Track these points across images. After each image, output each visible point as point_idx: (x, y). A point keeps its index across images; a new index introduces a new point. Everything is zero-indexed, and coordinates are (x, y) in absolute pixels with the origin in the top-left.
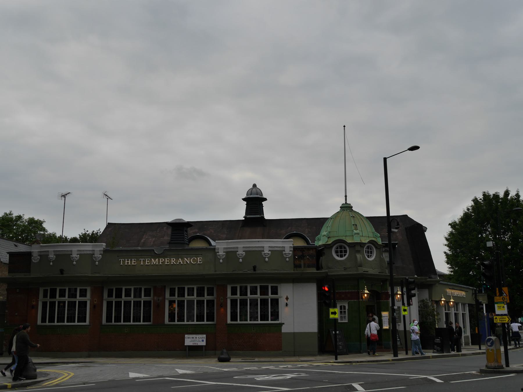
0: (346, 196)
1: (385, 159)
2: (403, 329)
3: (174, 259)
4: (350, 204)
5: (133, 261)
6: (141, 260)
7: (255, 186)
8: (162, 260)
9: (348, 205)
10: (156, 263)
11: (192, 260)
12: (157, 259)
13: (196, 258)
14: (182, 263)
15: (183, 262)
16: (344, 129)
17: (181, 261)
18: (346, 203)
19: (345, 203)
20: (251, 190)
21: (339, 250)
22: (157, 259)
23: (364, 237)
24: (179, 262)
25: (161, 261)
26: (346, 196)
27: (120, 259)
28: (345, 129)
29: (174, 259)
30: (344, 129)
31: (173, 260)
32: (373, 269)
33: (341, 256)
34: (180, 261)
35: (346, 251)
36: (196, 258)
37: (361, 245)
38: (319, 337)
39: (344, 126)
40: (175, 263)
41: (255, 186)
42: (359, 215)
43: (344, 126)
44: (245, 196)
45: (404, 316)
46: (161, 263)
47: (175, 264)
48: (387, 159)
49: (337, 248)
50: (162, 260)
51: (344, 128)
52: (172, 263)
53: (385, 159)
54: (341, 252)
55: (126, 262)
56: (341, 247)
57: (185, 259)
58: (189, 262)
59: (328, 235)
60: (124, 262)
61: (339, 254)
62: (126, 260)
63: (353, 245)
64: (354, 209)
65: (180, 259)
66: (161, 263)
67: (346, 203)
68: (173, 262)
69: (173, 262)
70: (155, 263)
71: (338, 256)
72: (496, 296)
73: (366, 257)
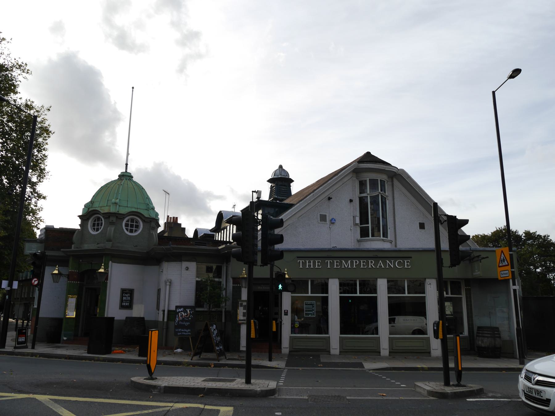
0: (127, 165)
1: (494, 93)
2: (161, 320)
3: (373, 261)
4: (130, 173)
5: (317, 264)
6: (300, 262)
7: (281, 167)
8: (356, 262)
9: (128, 174)
10: (348, 266)
11: (398, 262)
12: (349, 261)
13: (402, 261)
14: (383, 267)
15: (385, 265)
16: (133, 90)
17: (382, 265)
18: (126, 171)
19: (125, 171)
20: (274, 173)
21: (130, 223)
22: (349, 261)
23: (108, 206)
24: (379, 265)
25: (354, 264)
26: (127, 165)
27: (326, 261)
28: (134, 91)
29: (372, 262)
30: (133, 90)
31: (372, 262)
32: (134, 246)
33: (131, 231)
34: (380, 264)
35: (137, 227)
36: (402, 261)
37: (117, 217)
38: (439, 312)
39: (133, 88)
40: (374, 267)
41: (281, 167)
42: (140, 189)
43: (133, 88)
44: (270, 177)
45: (515, 291)
46: (378, 266)
47: (374, 268)
48: (495, 92)
49: (128, 221)
50: (356, 262)
51: (132, 89)
52: (370, 267)
53: (494, 93)
54: (132, 226)
55: (307, 264)
56: (132, 220)
57: (388, 261)
58: (392, 266)
59: (90, 205)
60: (304, 264)
61: (96, 227)
62: (307, 261)
63: (108, 215)
64: (134, 179)
65: (380, 261)
66: (378, 266)
67: (126, 171)
68: (371, 265)
69: (371, 265)
70: (346, 266)
71: (136, 231)
72: (256, 265)
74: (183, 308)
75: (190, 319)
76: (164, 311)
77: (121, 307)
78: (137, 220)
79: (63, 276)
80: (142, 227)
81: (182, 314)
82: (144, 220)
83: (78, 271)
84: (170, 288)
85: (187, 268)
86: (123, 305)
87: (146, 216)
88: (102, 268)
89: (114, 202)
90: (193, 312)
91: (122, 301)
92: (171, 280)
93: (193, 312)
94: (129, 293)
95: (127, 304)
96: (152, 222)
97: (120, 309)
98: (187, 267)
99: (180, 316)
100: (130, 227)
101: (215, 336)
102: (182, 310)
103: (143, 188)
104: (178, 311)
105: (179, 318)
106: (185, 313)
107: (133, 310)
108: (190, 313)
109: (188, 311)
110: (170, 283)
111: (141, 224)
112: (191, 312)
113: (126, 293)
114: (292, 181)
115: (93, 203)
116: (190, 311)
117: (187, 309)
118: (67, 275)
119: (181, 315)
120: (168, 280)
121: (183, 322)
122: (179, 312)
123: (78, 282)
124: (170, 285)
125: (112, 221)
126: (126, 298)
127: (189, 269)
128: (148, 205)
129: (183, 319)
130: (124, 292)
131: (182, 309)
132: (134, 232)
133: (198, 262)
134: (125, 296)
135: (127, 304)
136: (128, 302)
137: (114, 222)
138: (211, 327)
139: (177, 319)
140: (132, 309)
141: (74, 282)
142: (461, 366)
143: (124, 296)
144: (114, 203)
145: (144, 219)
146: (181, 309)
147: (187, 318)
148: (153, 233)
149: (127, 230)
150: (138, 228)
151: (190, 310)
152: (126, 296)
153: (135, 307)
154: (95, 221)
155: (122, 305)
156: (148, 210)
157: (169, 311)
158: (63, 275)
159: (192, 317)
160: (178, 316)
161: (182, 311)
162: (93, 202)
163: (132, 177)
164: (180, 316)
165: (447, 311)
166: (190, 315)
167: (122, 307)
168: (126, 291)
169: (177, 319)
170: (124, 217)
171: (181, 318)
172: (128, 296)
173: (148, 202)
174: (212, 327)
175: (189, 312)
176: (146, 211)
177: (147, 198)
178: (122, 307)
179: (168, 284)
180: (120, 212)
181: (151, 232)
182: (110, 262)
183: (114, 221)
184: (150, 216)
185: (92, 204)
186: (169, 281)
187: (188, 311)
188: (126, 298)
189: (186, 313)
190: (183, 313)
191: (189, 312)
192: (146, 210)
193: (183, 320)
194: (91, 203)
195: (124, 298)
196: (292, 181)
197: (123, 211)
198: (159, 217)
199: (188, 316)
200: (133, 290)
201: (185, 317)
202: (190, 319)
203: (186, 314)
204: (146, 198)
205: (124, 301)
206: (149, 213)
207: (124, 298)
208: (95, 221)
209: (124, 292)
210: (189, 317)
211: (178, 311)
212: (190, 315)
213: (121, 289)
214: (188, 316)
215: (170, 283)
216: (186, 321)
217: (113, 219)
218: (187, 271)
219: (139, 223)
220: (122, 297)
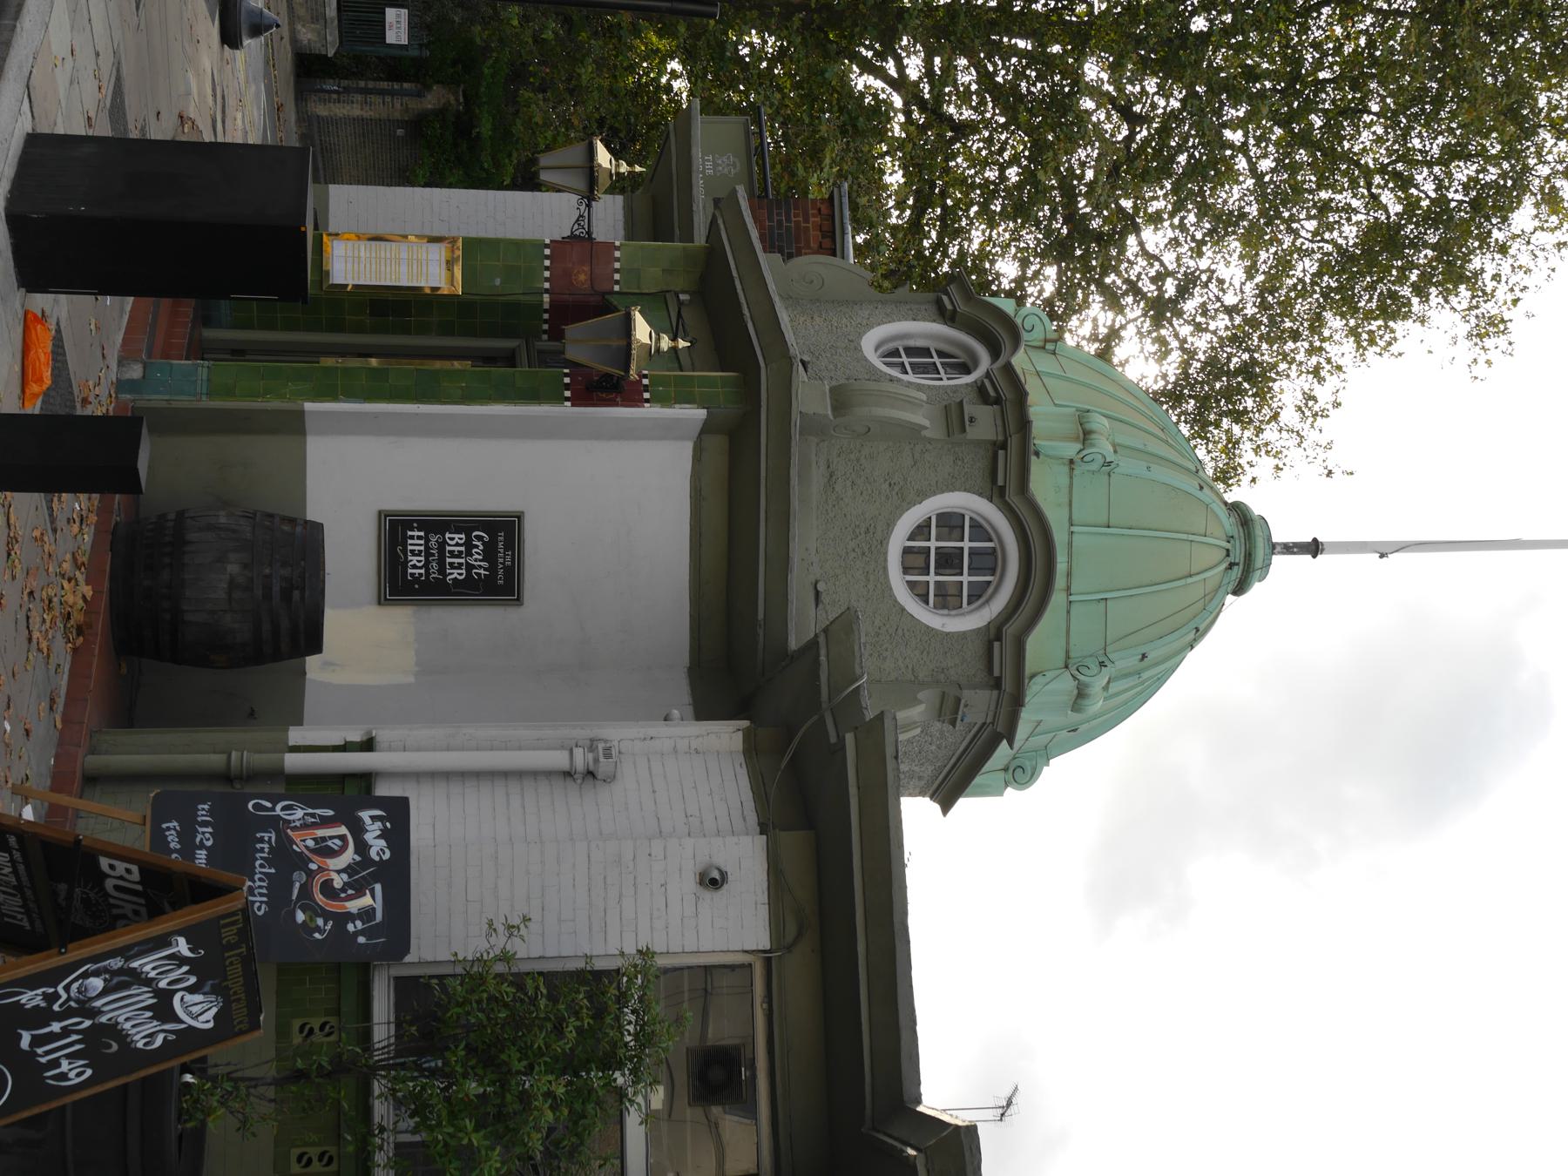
4: (1267, 566)
18: (1273, 548)
21: (966, 545)
33: (914, 560)
35: (946, 600)
49: (980, 530)
56: (988, 561)
67: (1273, 548)
73: (898, 539)
74: (387, 856)
75: (300, 917)
76: (368, 745)
77: (395, 590)
78: (990, 590)
79: (583, 208)
80: (948, 629)
81: (333, 853)
82: (999, 638)
83: (617, 288)
84: (549, 774)
85: (716, 875)
86: (405, 538)
87: (1032, 643)
88: (658, 339)
89: (1093, 426)
90: (361, 940)
91: (436, 524)
92: (610, 779)
93: (361, 940)
94: (492, 568)
95: (414, 560)
96: (995, 692)
97: (383, 515)
98: (724, 875)
99: (321, 833)
100: (937, 548)
101: (84, 1008)
102: (373, 854)
103: (1199, 634)
104: (365, 815)
105: (305, 826)
106: (345, 877)
107: (375, 610)
108: (350, 917)
109: (366, 901)
110: (590, 774)
111: (968, 618)
112: (359, 924)
113: (490, 554)
114: (1314, 557)
115: (1048, 352)
116: (367, 914)
117: (378, 887)
118: (589, 233)
119: (335, 844)
120: (608, 755)
121: (268, 862)
122: (358, 829)
123: (546, 298)
124: (568, 774)
125: (972, 420)
126: (459, 555)
127: (708, 895)
128: (1102, 664)
129: (301, 862)
130: (501, 537)
131: (378, 847)
132: (908, 582)
133: (768, 961)
134: (469, 546)
135: (414, 560)
136: (426, 566)
137: (964, 430)
138: (182, 946)
139: (299, 813)
140: (382, 601)
141: (546, 316)
142: (1001, 645)
143: (469, 539)
144: (1088, 426)
145: (1010, 630)
146: (382, 843)
147: (306, 890)
148: (915, 702)
149: (921, 531)
150: (935, 607)
151: (379, 916)
152: (469, 554)
153: (401, 620)
154: (941, 354)
155: (408, 525)
156: (1066, 667)
157: (366, 779)
158: (589, 206)
159: (318, 929)
160: (325, 822)
161: (362, 847)
162: (1054, 353)
163: (1240, 589)
164: (321, 833)
165: (580, 11)
166: (327, 916)
167: (395, 528)
168: (509, 545)
169: (299, 813)
170: (1002, 490)
171: (303, 842)
172: (470, 567)
173: (1120, 664)
174: (195, 966)
175: (354, 906)
176: (1062, 655)
177: (1144, 656)
178: (395, 528)
179: (581, 759)
180: (1035, 466)
181: (920, 696)
182: (702, 413)
183: (973, 433)
184: (1033, 676)
185: (1044, 348)
186: (604, 767)
187: (366, 901)
188: (459, 555)
189: (346, 886)
190: (349, 856)
191: (354, 906)
192: (1068, 657)
193: (287, 859)
194: (1046, 341)
195: (456, 539)
196: (1314, 557)
197: (1045, 484)
198: (1009, 790)
199: (319, 898)
200: (519, 601)
201: (311, 874)
202: (300, 917)
203: (338, 881)
204: (1143, 649)
205: (434, 539)
206: (1050, 675)
207: (460, 538)
208: (941, 354)
209: (501, 537)
210: (313, 910)
211: (365, 815)
212: (327, 916)
213: (519, 516)
214: (319, 898)
215: (590, 774)
216: (278, 889)
217: (985, 420)
218: (690, 883)
219: (973, 606)
220: (465, 523)
